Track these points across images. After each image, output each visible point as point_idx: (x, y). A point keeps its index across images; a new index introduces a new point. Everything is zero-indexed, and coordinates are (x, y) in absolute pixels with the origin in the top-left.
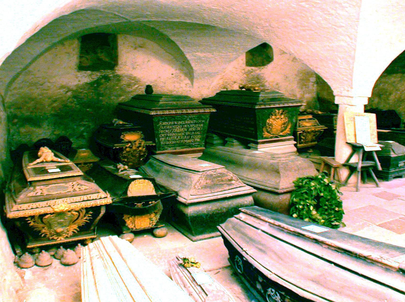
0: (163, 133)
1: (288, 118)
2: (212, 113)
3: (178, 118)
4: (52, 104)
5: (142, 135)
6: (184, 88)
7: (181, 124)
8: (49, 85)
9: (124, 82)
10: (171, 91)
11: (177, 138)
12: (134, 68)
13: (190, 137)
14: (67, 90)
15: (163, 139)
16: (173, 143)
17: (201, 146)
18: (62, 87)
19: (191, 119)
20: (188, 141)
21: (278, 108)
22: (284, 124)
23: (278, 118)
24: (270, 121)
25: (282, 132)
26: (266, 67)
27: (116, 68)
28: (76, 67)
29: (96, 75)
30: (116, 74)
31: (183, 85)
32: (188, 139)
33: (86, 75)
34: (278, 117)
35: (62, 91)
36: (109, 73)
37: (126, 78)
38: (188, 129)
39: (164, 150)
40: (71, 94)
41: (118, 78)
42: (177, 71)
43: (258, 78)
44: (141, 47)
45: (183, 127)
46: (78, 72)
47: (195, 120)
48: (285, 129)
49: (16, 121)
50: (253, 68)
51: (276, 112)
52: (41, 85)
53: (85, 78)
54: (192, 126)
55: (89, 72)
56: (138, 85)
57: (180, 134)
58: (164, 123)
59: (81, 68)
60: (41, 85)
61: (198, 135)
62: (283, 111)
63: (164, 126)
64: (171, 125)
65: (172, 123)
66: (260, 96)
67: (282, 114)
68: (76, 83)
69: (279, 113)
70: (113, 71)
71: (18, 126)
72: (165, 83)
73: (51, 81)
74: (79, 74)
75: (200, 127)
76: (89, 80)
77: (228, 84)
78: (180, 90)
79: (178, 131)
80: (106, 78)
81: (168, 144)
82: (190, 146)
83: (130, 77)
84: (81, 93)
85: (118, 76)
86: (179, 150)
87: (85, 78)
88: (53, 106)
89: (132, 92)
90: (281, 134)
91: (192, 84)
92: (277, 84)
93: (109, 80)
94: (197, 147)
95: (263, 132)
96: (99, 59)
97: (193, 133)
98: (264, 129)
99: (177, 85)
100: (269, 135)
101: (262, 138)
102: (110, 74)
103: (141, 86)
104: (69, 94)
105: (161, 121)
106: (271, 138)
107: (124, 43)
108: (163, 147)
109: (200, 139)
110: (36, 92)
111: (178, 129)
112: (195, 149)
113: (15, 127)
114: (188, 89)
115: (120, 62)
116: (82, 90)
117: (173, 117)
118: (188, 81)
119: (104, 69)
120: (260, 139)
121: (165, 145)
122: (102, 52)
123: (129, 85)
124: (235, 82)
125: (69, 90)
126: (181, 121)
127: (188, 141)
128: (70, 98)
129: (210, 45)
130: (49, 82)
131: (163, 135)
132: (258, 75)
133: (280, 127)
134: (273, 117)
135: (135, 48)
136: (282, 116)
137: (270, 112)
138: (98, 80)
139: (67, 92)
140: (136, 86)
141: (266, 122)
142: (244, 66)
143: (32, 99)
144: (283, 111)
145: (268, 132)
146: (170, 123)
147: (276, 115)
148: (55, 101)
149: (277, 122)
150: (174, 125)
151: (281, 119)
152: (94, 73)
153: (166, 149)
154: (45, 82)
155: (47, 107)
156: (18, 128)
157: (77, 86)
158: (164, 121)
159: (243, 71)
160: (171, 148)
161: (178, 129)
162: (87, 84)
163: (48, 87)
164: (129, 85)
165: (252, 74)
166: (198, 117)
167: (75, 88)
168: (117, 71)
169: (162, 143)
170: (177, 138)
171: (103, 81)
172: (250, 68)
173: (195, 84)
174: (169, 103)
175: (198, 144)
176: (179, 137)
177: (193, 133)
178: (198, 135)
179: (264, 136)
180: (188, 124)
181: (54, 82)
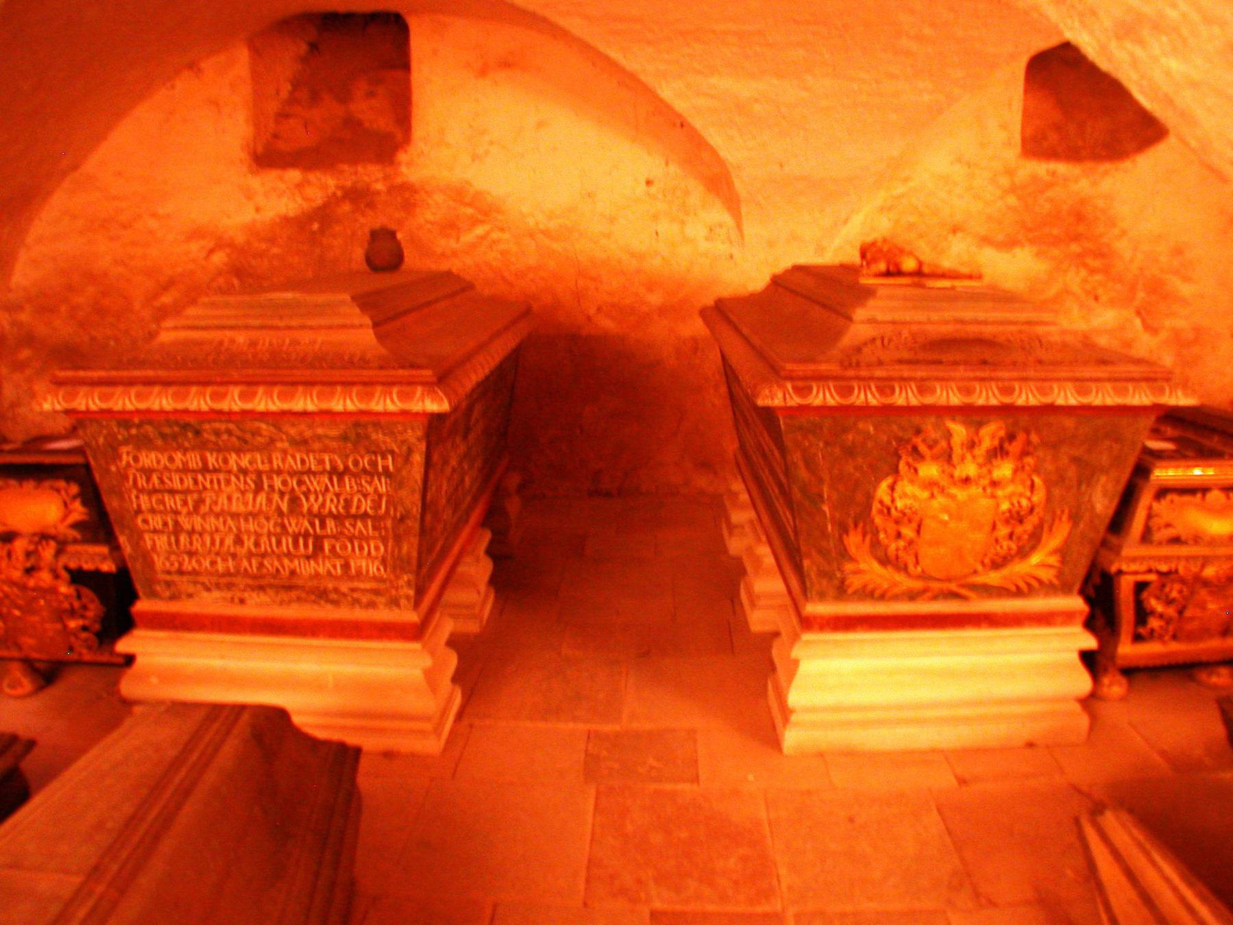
0: (153, 511)
1: (1049, 485)
2: (435, 420)
3: (217, 433)
4: (156, 296)
5: (77, 505)
6: (704, 246)
7: (244, 472)
8: (153, 224)
9: (430, 213)
10: (641, 257)
11: (239, 541)
12: (475, 157)
13: (319, 547)
14: (212, 245)
15: (162, 542)
16: (220, 567)
17: (394, 602)
18: (196, 233)
19: (302, 443)
20: (307, 569)
21: (973, 415)
22: (1015, 517)
23: (967, 481)
24: (907, 493)
25: (996, 565)
26: (1127, 164)
27: (402, 157)
28: (244, 156)
29: (323, 186)
30: (399, 180)
31: (696, 230)
32: (308, 558)
33: (282, 186)
34: (970, 469)
35: (194, 247)
36: (372, 176)
37: (439, 198)
38: (294, 501)
39: (173, 598)
40: (225, 259)
41: (407, 196)
42: (674, 169)
43: (1079, 217)
44: (506, 64)
45: (259, 488)
46: (252, 172)
47: (326, 450)
48: (1023, 554)
49: (25, 353)
50: (1062, 168)
51: (948, 435)
52: (125, 226)
53: (279, 198)
54: (315, 484)
55: (294, 175)
56: (486, 227)
57: (252, 526)
58: (149, 459)
59: (266, 158)
60: (125, 226)
61: (363, 538)
62: (1011, 437)
63: (148, 472)
64: (185, 470)
65: (194, 460)
66: (860, 314)
67: (999, 452)
68: (247, 215)
69: (971, 445)
70: (389, 170)
71: (28, 372)
72: (612, 220)
73: (161, 211)
74: (255, 182)
75: (367, 494)
76: (292, 206)
77: (921, 236)
78: (684, 250)
79: (237, 507)
80: (359, 197)
81: (194, 572)
82: (321, 595)
83: (459, 193)
84: (261, 255)
85: (407, 187)
86: (258, 606)
87: (279, 198)
88: (157, 304)
89: (455, 254)
90: (993, 578)
91: (739, 227)
92: (1178, 251)
93: (371, 205)
94: (372, 605)
95: (844, 554)
96: (352, 123)
97: (330, 524)
98: (853, 541)
99: (666, 228)
100: (900, 577)
101: (842, 592)
102: (377, 181)
103: (502, 230)
104: (219, 258)
105: (126, 442)
106: (912, 596)
107: (435, 52)
108: (168, 584)
109: (384, 561)
110: (105, 254)
111: (232, 496)
112: (359, 614)
113: (17, 376)
114: (721, 247)
115: (418, 132)
116: (263, 246)
117: (186, 427)
118: (718, 214)
119: (355, 162)
120: (822, 596)
121: (181, 572)
122: (371, 95)
123: (450, 227)
124: (955, 230)
125: (221, 243)
126: (239, 451)
127: (307, 569)
128: (220, 273)
129: (760, 33)
130: (154, 215)
131: (156, 522)
132: (1083, 202)
133: (980, 537)
134: (930, 470)
135: (483, 72)
136: (1004, 470)
137: (903, 439)
138: (325, 206)
139: (211, 251)
140: (480, 230)
141: (870, 497)
142: (1012, 154)
143: (92, 278)
144: (1011, 437)
145: (884, 561)
146: (178, 456)
147: (947, 457)
148: (170, 284)
149: (953, 497)
150: (205, 469)
151: (995, 484)
152: (312, 176)
153: (190, 596)
154: (140, 216)
155: (137, 306)
156: (29, 380)
157: (250, 229)
158: (143, 443)
159: (1004, 181)
160: (216, 594)
161: (232, 496)
162: (286, 220)
163: (151, 232)
164: (450, 227)
165: (1049, 194)
166: (344, 438)
167: (240, 239)
168: (404, 169)
169: (159, 562)
170: (239, 541)
171: (346, 207)
172: (1041, 168)
173: (751, 229)
174: (200, 343)
175: (377, 592)
176: (249, 543)
177: (330, 524)
178: (363, 538)
179: (855, 582)
180: (292, 473)
181: (168, 216)
